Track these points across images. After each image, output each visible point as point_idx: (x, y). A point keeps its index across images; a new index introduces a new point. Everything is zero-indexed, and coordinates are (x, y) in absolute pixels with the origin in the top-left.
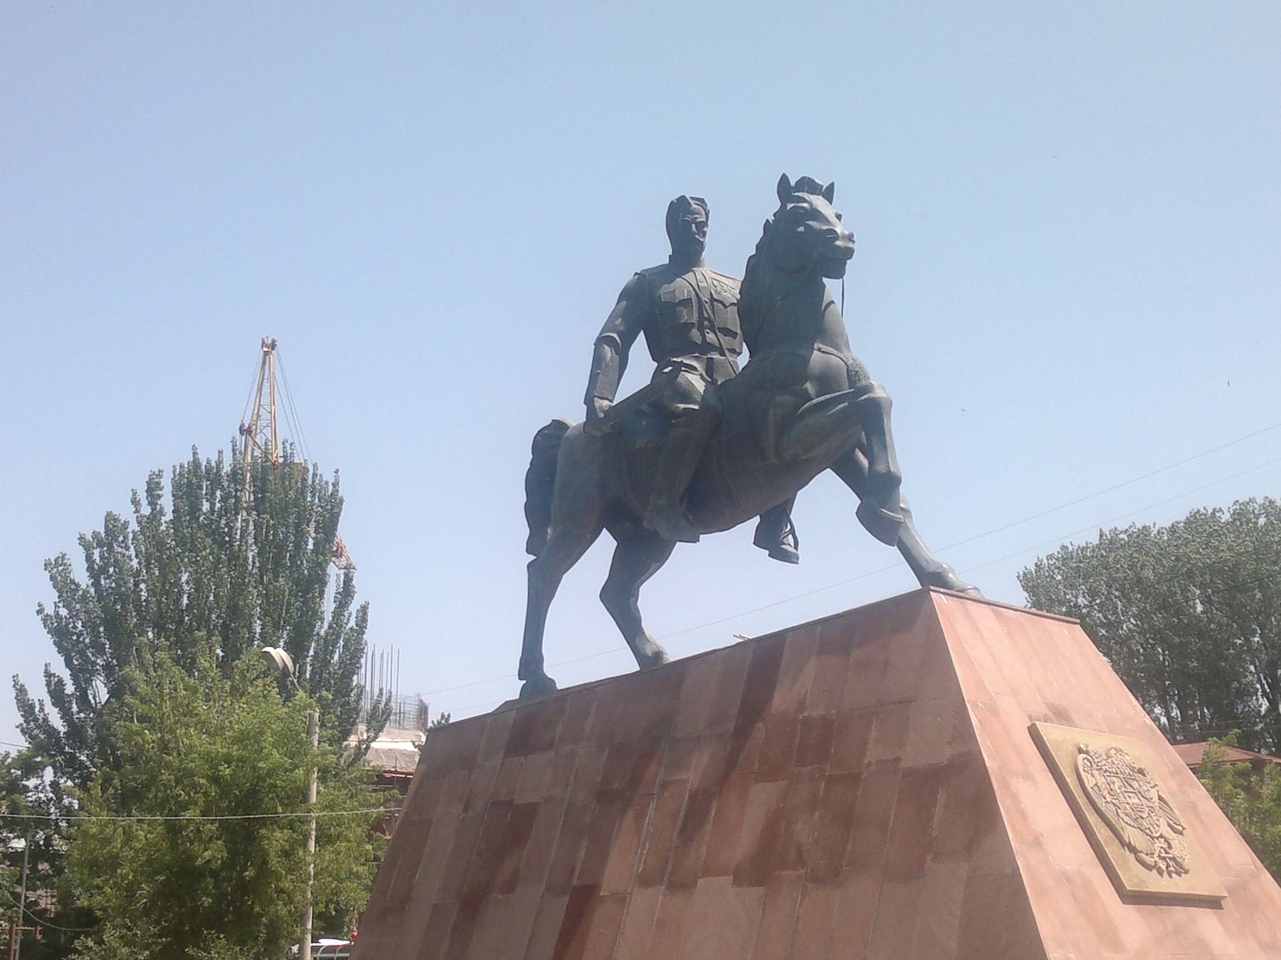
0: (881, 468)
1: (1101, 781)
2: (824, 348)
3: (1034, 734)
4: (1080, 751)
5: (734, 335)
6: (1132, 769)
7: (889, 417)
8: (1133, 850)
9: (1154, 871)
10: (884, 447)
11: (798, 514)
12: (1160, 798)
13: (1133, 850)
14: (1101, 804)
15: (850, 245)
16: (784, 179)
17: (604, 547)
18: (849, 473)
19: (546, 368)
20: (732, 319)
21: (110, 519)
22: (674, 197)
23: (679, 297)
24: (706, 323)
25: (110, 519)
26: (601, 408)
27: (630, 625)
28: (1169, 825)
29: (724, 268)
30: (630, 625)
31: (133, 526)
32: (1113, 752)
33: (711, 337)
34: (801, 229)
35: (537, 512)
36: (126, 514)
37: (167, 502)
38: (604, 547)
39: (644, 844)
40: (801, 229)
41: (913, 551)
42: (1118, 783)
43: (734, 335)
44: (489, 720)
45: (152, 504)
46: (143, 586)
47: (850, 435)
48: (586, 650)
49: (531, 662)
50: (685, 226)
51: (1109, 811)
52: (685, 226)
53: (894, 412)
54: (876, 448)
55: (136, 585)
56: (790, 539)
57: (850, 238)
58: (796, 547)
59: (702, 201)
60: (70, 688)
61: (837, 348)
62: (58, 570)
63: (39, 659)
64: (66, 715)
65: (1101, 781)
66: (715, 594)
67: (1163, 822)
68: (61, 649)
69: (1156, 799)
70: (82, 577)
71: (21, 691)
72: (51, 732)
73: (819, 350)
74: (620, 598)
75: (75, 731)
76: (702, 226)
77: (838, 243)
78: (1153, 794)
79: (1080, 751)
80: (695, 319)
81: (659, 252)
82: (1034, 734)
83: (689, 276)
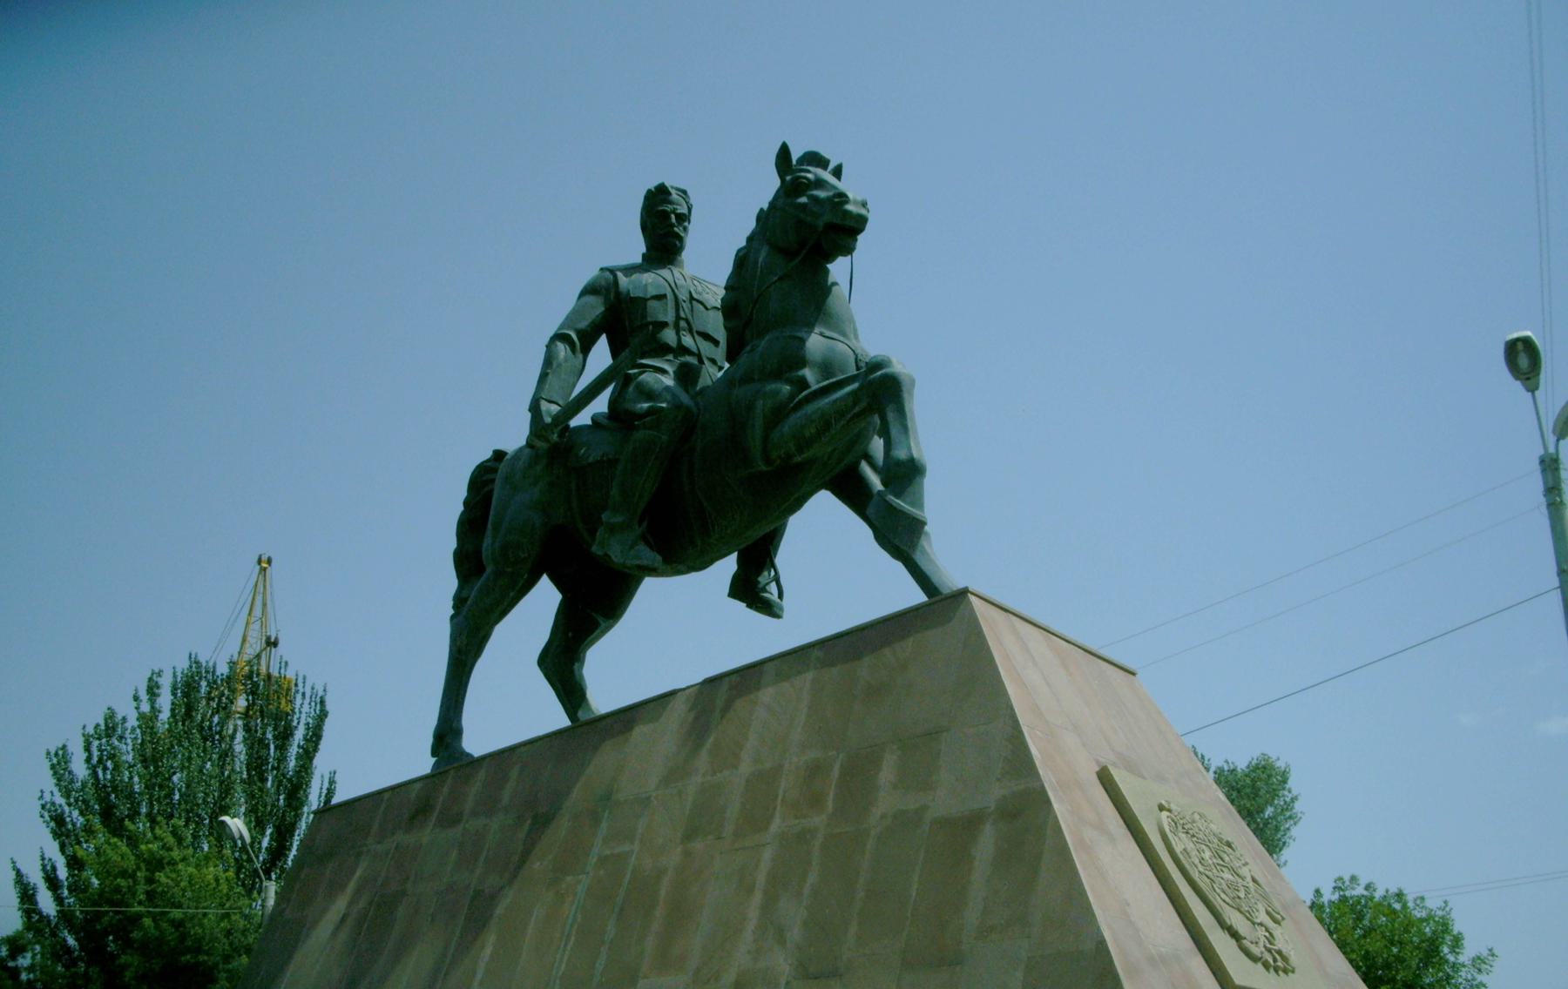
0: (900, 454)
1: (1190, 846)
2: (828, 333)
3: (1105, 778)
4: (1161, 808)
5: (716, 343)
6: (1220, 840)
7: (911, 394)
8: (1235, 935)
9: (1260, 964)
10: (905, 429)
11: (785, 557)
12: (1254, 880)
13: (1235, 935)
14: (1195, 876)
15: (863, 212)
16: (784, 153)
17: (543, 601)
18: (853, 493)
19: (484, 386)
20: (715, 324)
21: (110, 716)
22: (652, 185)
23: (652, 292)
24: (683, 324)
25: (110, 716)
26: (549, 412)
27: (570, 691)
28: (1268, 913)
29: (708, 263)
30: (570, 691)
31: (133, 721)
32: (1197, 817)
33: (687, 340)
34: (803, 200)
35: (468, 562)
36: (129, 714)
37: (165, 701)
38: (543, 601)
39: (569, 936)
40: (803, 200)
41: (935, 579)
42: (1207, 855)
43: (716, 343)
44: (386, 796)
45: (152, 701)
46: (136, 779)
47: (851, 442)
48: (511, 705)
49: (447, 735)
50: (663, 225)
51: (1203, 884)
52: (663, 225)
53: (916, 391)
54: (894, 431)
55: (131, 778)
56: (773, 587)
57: (864, 205)
58: (781, 596)
59: (685, 192)
60: (63, 873)
61: (844, 334)
62: (59, 764)
63: (37, 847)
64: (59, 900)
65: (1190, 846)
66: (677, 630)
67: (1261, 907)
68: (56, 835)
69: (1249, 879)
70: (80, 769)
71: (20, 879)
72: (44, 918)
73: (821, 334)
74: (561, 664)
75: (65, 916)
76: (683, 218)
77: (849, 207)
78: (1244, 871)
79: (1161, 808)
80: (670, 317)
81: (634, 248)
82: (1105, 778)
83: (665, 273)
